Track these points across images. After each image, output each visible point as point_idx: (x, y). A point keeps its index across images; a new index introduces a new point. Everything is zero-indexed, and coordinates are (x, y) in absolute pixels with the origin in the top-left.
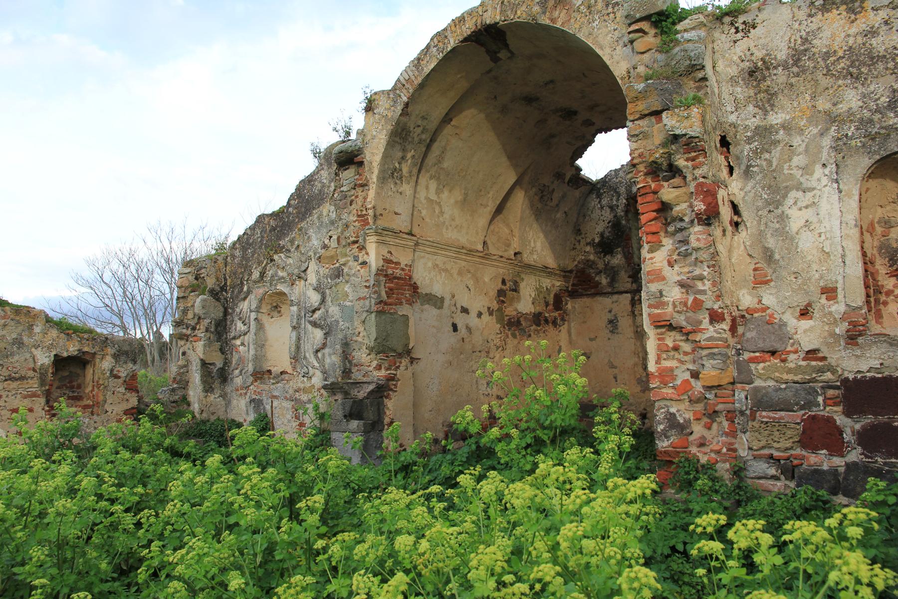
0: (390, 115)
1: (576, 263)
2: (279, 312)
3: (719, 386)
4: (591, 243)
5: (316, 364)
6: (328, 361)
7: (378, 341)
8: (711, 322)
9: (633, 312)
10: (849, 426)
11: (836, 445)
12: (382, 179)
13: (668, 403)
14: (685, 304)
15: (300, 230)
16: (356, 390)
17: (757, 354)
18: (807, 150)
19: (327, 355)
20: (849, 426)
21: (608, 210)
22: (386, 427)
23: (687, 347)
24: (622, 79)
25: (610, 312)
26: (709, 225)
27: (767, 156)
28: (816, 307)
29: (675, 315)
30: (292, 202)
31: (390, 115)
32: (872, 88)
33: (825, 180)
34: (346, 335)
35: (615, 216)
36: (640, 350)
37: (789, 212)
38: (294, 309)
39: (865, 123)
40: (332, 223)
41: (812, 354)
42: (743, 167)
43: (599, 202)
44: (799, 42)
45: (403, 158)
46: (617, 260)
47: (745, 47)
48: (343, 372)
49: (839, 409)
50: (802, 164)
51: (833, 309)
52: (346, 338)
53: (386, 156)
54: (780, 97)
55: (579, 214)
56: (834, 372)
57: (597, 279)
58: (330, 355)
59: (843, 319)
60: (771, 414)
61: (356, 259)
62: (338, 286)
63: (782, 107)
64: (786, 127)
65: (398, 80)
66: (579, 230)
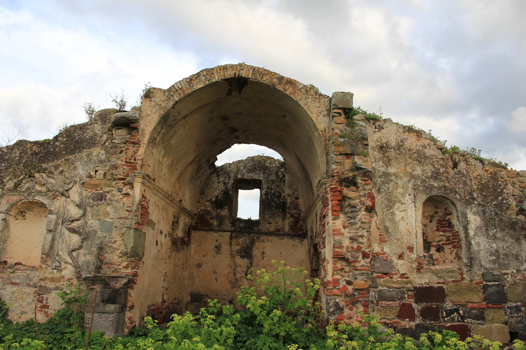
0: (163, 105)
1: (199, 210)
2: (24, 216)
3: (361, 290)
4: (210, 201)
5: (70, 261)
6: (82, 259)
7: (134, 249)
9: (231, 243)
10: (417, 307)
11: (412, 318)
12: (149, 143)
13: (334, 297)
15: (67, 160)
16: (114, 282)
17: (380, 274)
18: (403, 187)
19: (81, 255)
20: (417, 307)
21: (223, 184)
22: (128, 309)
23: (347, 269)
24: (321, 131)
25: (217, 241)
26: (370, 212)
27: (387, 185)
28: (405, 255)
29: (347, 253)
30: (60, 139)
31: (163, 105)
32: (425, 168)
33: (410, 201)
34: (102, 241)
35: (226, 188)
37: (396, 212)
38: (54, 217)
39: (423, 181)
40: (101, 162)
41: (403, 276)
42: (377, 188)
43: (218, 179)
44: (400, 141)
45: (160, 132)
46: (224, 212)
47: (379, 135)
48: (96, 268)
49: (413, 300)
52: (102, 244)
53: (155, 129)
54: (393, 161)
56: (412, 284)
57: (211, 221)
58: (85, 255)
59: (415, 261)
60: (386, 303)
61: (120, 190)
62: (99, 206)
63: (394, 166)
64: (395, 175)
65: (173, 86)
66: (203, 192)
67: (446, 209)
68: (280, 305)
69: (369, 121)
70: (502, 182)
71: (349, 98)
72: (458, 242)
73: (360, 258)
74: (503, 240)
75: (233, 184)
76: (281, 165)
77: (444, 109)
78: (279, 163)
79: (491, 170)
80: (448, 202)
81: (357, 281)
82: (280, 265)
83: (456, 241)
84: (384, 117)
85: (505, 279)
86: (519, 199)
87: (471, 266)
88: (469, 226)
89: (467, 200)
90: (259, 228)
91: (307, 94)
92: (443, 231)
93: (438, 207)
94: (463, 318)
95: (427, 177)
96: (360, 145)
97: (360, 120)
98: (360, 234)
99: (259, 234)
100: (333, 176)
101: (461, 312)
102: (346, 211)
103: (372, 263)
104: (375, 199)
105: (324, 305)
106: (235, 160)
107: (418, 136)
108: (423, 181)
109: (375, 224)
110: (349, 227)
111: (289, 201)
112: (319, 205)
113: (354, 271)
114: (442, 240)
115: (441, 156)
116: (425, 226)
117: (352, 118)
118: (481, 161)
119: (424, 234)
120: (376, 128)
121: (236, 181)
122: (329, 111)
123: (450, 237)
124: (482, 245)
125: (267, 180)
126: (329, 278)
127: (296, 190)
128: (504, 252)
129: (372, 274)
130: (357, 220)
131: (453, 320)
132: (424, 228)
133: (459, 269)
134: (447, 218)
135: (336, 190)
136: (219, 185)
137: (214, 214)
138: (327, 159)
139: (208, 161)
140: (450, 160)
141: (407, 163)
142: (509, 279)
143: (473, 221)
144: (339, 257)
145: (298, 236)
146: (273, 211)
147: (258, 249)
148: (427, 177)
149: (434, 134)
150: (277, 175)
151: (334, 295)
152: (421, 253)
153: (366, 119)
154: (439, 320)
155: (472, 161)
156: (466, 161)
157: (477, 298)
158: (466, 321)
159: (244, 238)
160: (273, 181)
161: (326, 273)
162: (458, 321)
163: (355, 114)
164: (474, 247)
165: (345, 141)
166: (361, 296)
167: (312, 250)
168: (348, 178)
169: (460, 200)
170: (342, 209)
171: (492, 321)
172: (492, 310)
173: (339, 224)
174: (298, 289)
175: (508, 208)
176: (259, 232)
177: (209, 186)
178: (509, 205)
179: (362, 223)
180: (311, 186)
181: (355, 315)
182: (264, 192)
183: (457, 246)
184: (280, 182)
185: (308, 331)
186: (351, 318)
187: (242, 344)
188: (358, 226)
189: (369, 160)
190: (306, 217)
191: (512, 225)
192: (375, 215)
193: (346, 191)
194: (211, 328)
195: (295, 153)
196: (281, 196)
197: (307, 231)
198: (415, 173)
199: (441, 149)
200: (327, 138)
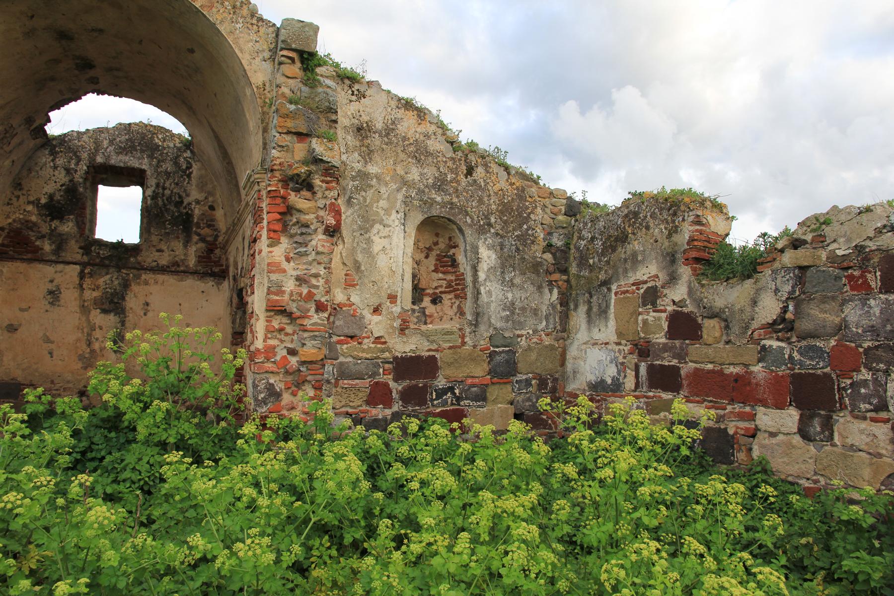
1: (10, 221)
3: (311, 362)
4: (36, 203)
8: (317, 311)
11: (388, 403)
13: (267, 375)
14: (300, 295)
18: (388, 198)
21: (63, 172)
23: (289, 329)
25: (52, 281)
26: (332, 236)
27: (364, 194)
28: (384, 307)
29: (290, 302)
32: (425, 171)
35: (71, 181)
36: (85, 325)
37: (374, 238)
42: (347, 197)
43: (53, 160)
46: (68, 227)
47: (357, 108)
49: (391, 377)
50: (385, 207)
51: (394, 309)
54: (376, 155)
55: (23, 166)
56: (390, 352)
57: (38, 243)
60: (350, 382)
64: (378, 177)
66: (20, 184)
67: (450, 239)
68: (172, 392)
69: (342, 80)
70: (531, 203)
71: (312, 33)
72: (463, 289)
73: (312, 312)
74: (522, 288)
75: (87, 173)
76: (185, 145)
77: (469, 85)
78: (181, 142)
79: (518, 184)
80: (455, 227)
81: (305, 349)
82: (175, 324)
83: (460, 287)
84: (369, 77)
85: (518, 343)
86: (549, 230)
87: (476, 325)
88: (480, 265)
89: (480, 226)
90: (139, 258)
91: (234, 13)
92: (443, 273)
93: (439, 234)
94: (459, 399)
95: (427, 186)
96: (323, 121)
97: (327, 77)
98: (313, 271)
99: (138, 269)
100: (272, 171)
101: (457, 391)
102: (292, 231)
103: (332, 319)
104: (340, 215)
105: (250, 390)
106: (92, 127)
107: (419, 116)
108: (420, 192)
109: (339, 256)
110: (296, 259)
111: (197, 212)
112: (249, 221)
113: (301, 333)
114: (441, 286)
115: (450, 154)
116: (418, 263)
117: (313, 70)
118: (507, 168)
119: (414, 276)
120: (353, 94)
121: (94, 167)
122: (274, 51)
123: (452, 281)
124: (493, 294)
125: (156, 171)
126: (259, 344)
127: (210, 194)
128: (521, 305)
129: (331, 337)
130: (310, 248)
131: (445, 403)
132: (416, 266)
133: (460, 329)
134: (451, 253)
135: (278, 194)
136: (56, 173)
137: (45, 229)
138: (264, 138)
139: (29, 121)
140: (463, 162)
141: (399, 160)
142: (523, 342)
143: (486, 258)
144: (276, 310)
145: (213, 275)
146: (166, 229)
147: (136, 297)
148: (427, 186)
149: (445, 119)
150: (176, 163)
151: (266, 372)
152: (408, 305)
153: (339, 76)
154: (425, 403)
155: (494, 168)
156: (486, 166)
157: (479, 371)
158: (462, 403)
159: (108, 276)
160: (168, 174)
161: (253, 337)
162: (452, 404)
163: (320, 65)
164: (484, 298)
165: (298, 109)
166: (312, 372)
167: (235, 300)
168: (298, 175)
169: (470, 226)
170: (285, 229)
171: (495, 401)
172: (496, 387)
173: (280, 254)
174: (205, 365)
175: (533, 242)
176: (137, 266)
177: (33, 173)
178: (536, 238)
179: (318, 253)
180: (237, 185)
181: (300, 404)
182: (149, 192)
183: (461, 296)
184: (182, 176)
185: (220, 433)
186: (293, 408)
187: (96, 464)
188: (310, 258)
189: (336, 147)
190: (227, 241)
191: (536, 267)
192: (340, 242)
193: (294, 199)
194: (18, 438)
195: (210, 126)
196: (182, 202)
197: (228, 267)
198: (410, 177)
199: (452, 143)
200: (267, 100)
